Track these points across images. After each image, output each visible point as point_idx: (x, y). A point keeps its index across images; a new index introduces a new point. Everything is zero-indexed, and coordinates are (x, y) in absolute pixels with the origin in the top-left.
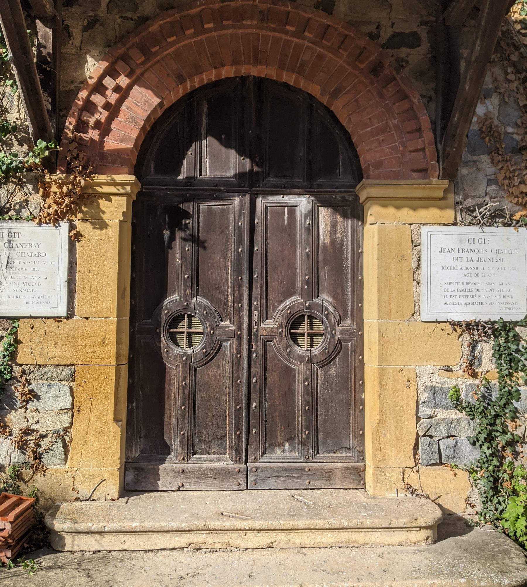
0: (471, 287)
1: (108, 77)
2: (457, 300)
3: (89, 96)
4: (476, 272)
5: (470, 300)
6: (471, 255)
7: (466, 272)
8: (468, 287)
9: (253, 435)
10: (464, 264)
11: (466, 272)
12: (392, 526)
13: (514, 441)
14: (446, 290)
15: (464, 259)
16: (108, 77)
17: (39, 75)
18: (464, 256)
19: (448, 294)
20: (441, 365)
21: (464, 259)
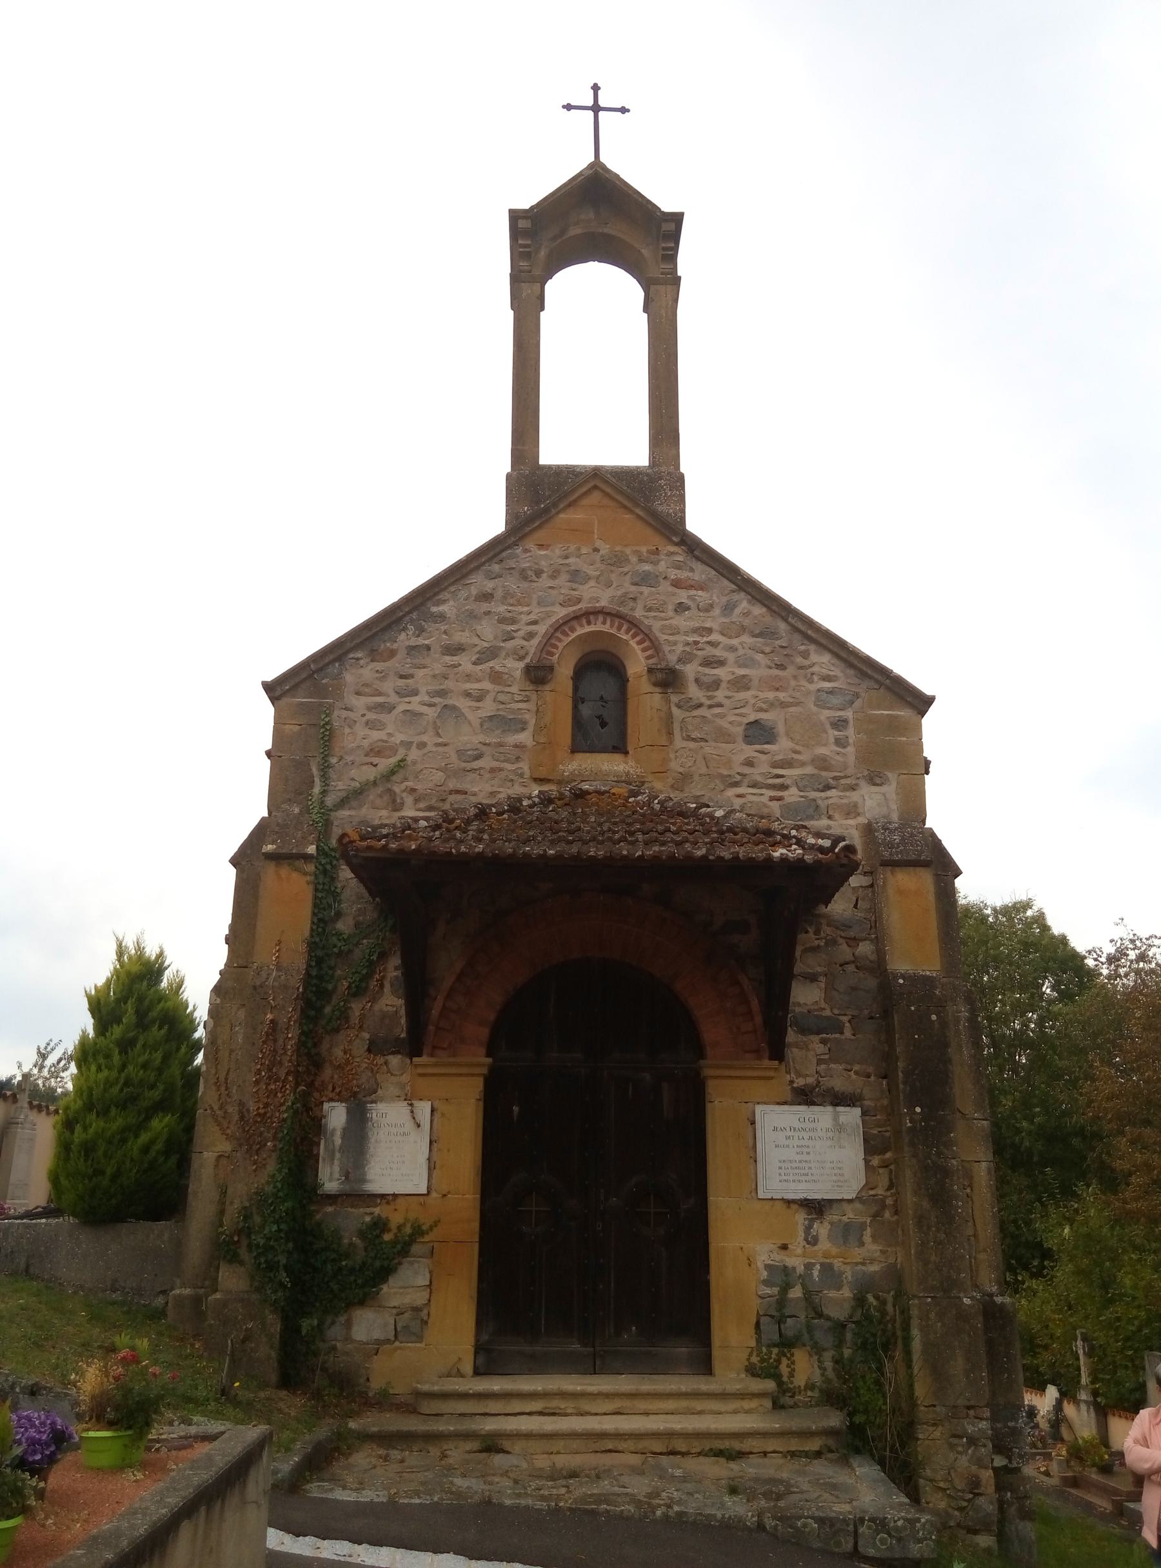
0: (804, 1164)
1: (541, 463)
2: (791, 1178)
3: (820, 974)
4: (807, 1150)
5: (803, 1178)
6: (802, 1134)
7: (799, 1150)
8: (800, 1165)
9: (279, 847)
10: (796, 1142)
11: (799, 1150)
12: (771, 1203)
13: (856, 1430)
14: (780, 1168)
15: (796, 1138)
16: (541, 463)
17: (1023, 1356)
18: (796, 1134)
19: (782, 1172)
20: (780, 1242)
21: (796, 1138)
